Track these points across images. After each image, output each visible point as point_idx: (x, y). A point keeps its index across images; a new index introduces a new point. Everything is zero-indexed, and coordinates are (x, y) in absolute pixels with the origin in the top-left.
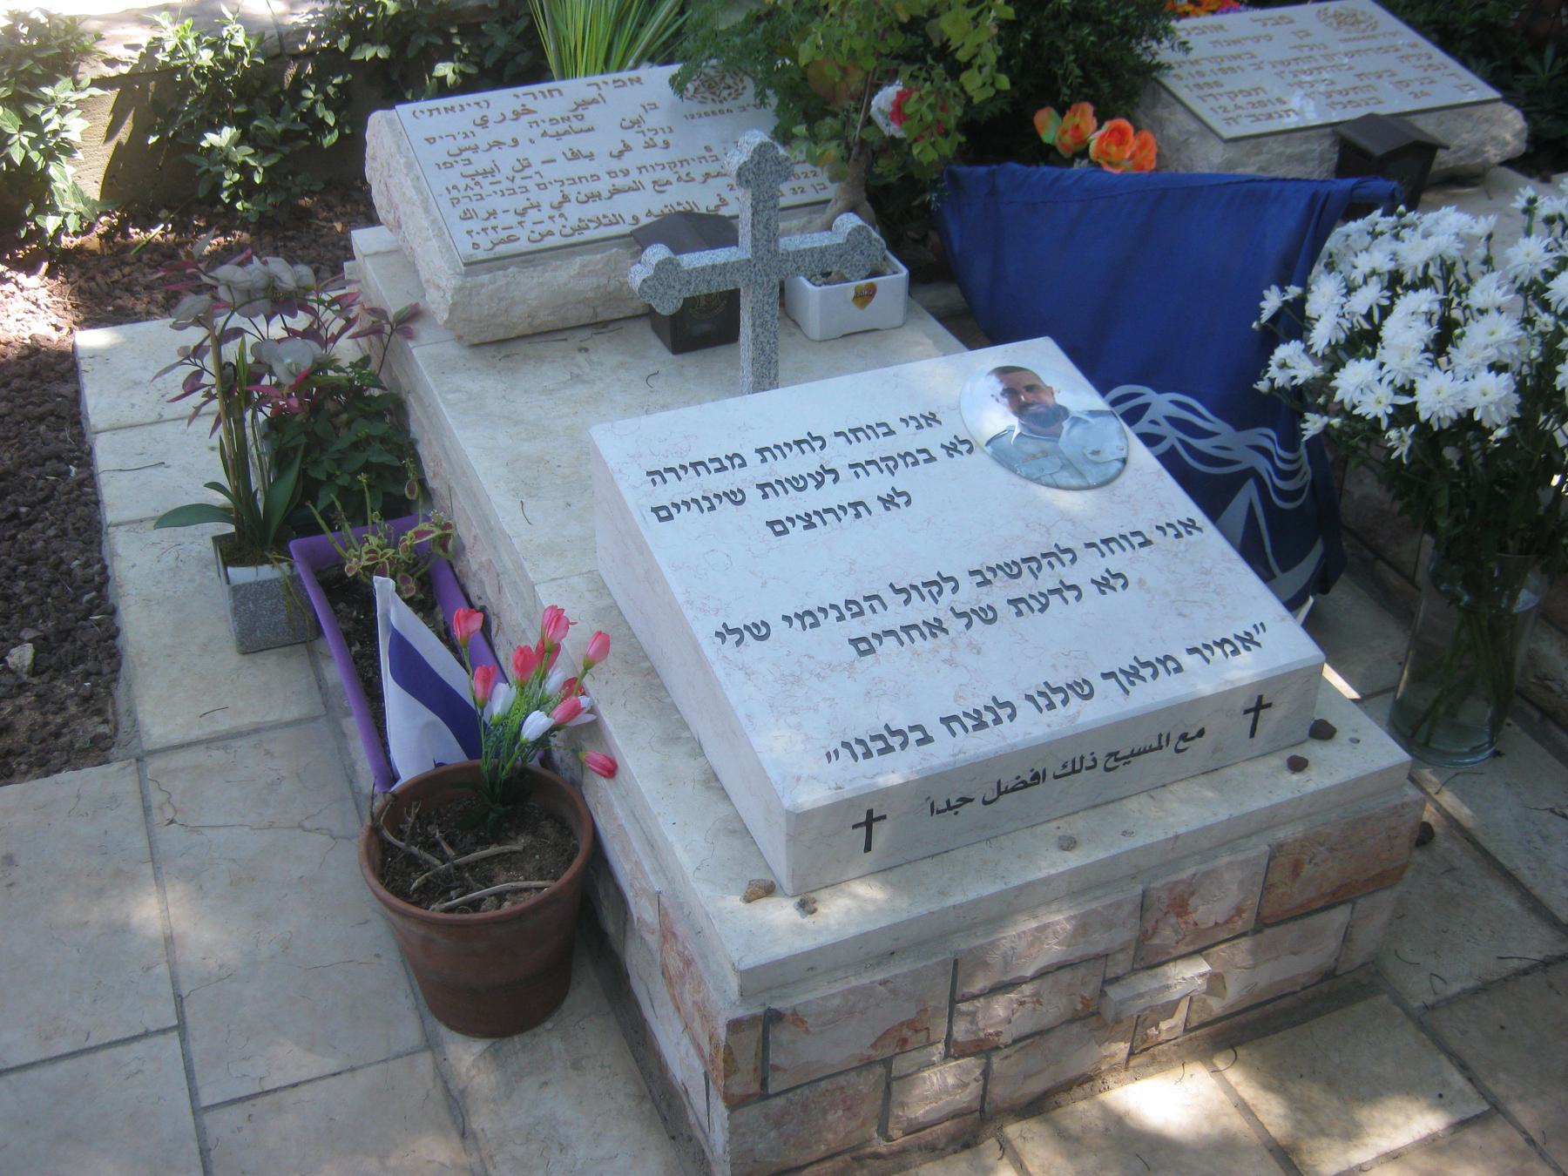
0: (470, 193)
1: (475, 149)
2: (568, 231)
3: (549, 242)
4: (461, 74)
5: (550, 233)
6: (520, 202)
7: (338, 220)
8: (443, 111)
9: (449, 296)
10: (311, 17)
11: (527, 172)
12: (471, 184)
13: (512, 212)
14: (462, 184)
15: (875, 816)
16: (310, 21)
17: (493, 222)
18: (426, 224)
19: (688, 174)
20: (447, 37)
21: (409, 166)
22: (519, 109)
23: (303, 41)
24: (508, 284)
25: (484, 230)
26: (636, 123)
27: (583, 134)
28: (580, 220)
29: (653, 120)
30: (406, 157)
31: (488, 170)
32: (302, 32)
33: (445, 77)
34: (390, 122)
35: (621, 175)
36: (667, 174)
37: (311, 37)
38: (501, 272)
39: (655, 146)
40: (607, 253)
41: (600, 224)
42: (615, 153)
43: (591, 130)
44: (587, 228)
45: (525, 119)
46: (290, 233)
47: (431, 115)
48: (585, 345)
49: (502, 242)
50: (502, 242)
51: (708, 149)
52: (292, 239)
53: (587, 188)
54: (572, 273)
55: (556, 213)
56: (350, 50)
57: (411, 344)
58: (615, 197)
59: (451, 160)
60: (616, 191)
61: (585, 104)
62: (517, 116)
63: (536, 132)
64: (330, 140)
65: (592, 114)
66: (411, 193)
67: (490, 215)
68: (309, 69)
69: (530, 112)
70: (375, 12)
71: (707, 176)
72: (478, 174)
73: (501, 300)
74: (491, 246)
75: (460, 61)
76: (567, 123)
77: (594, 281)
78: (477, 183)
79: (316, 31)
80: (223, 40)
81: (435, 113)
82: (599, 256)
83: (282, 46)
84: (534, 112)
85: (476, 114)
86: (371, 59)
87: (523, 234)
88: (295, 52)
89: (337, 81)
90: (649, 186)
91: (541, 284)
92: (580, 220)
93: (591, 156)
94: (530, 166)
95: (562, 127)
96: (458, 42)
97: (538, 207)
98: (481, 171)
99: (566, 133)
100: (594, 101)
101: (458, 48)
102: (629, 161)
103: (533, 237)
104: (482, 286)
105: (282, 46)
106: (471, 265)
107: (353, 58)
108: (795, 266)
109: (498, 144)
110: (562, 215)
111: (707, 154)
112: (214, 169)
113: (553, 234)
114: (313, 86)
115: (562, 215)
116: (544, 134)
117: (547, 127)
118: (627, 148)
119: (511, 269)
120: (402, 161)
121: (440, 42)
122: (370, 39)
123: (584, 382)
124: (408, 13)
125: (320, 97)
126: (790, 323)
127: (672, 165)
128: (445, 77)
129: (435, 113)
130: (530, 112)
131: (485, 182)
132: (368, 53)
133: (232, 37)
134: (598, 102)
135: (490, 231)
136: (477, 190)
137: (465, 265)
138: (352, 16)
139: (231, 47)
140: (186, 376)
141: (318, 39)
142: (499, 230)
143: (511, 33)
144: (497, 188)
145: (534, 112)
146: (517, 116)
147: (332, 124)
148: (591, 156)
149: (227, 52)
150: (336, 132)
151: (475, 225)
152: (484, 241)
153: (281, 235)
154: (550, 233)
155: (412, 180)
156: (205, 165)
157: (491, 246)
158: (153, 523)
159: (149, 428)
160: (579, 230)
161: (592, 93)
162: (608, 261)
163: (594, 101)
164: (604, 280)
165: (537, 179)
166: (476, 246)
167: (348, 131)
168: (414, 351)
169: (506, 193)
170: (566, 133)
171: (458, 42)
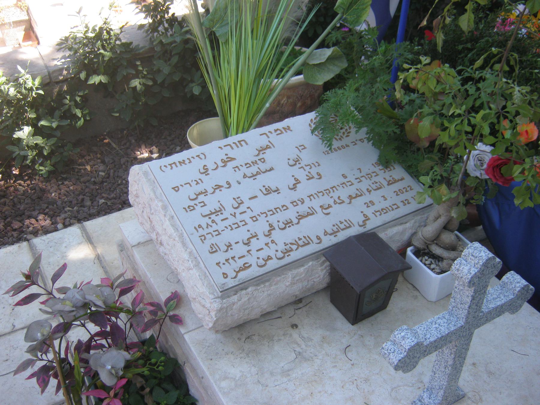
0: (210, 230)
1: (205, 193)
2: (280, 255)
3: (273, 264)
4: (144, 84)
5: (269, 258)
6: (242, 234)
7: (88, 164)
8: (178, 164)
9: (213, 314)
10: (63, 60)
11: (242, 208)
12: (210, 222)
13: (241, 243)
14: (204, 221)
15: (250, 252)
16: (64, 63)
17: (230, 254)
18: (186, 256)
19: (339, 198)
20: (135, 67)
21: (165, 208)
22: (225, 158)
23: (61, 75)
24: (249, 299)
25: (227, 260)
26: (297, 161)
27: (268, 173)
28: (286, 244)
29: (306, 157)
30: (161, 201)
31: (218, 209)
32: (61, 70)
33: (136, 87)
34: (146, 174)
35: (299, 203)
36: (326, 200)
37: (65, 72)
38: (244, 292)
39: (313, 178)
40: (306, 267)
41: (299, 246)
42: (291, 186)
43: (271, 169)
44: (292, 250)
45: (230, 165)
46: (65, 176)
47: (172, 168)
48: (295, 320)
49: (242, 269)
50: (242, 269)
51: (344, 176)
52: (66, 179)
53: (283, 216)
54: (287, 284)
55: (268, 240)
56: (87, 79)
57: (182, 330)
58: (301, 221)
59: (192, 203)
60: (300, 217)
61: (262, 150)
62: (225, 163)
63: (239, 175)
64: (81, 122)
65: (268, 155)
66: (171, 230)
67: (228, 246)
68: (65, 88)
69: (232, 159)
70: (99, 59)
71: (351, 197)
72: (212, 213)
73: (245, 310)
74: (235, 274)
75: (143, 78)
76: (256, 166)
77: (300, 285)
78: (213, 221)
79: (67, 69)
80: (21, 85)
81: (174, 166)
82: (302, 269)
83: (50, 78)
84: (234, 159)
85: (198, 164)
86: (98, 84)
87: (251, 260)
88: (57, 80)
89: (81, 94)
90: (319, 210)
91: (270, 295)
92: (286, 244)
93: (277, 191)
94: (242, 203)
95: (254, 169)
96: (141, 68)
97: (255, 236)
98: (213, 211)
99: (258, 173)
100: (268, 147)
101: (141, 72)
102: (304, 190)
103: (261, 262)
104: (234, 304)
105: (50, 78)
106: (226, 293)
107: (88, 83)
108: (486, 319)
109: (218, 187)
110: (273, 242)
111: (345, 181)
112: (22, 153)
113: (271, 258)
114: (68, 97)
115: (273, 242)
116: (245, 176)
117: (244, 169)
118: (298, 181)
119: (250, 289)
120: (160, 204)
121: (134, 72)
122: (96, 72)
123: (306, 360)
124: (115, 58)
125: (73, 103)
126: (410, 286)
127: (327, 191)
128: (136, 87)
129: (174, 166)
130: (232, 159)
131: (218, 219)
132: (96, 79)
133: (25, 83)
134: (270, 148)
135: (231, 261)
136: (215, 227)
137: (221, 292)
138: (86, 62)
139: (25, 88)
140: (28, 346)
141: (69, 73)
142: (236, 259)
143: (170, 65)
144: (226, 223)
145: (234, 159)
146: (225, 163)
147: (80, 116)
148: (277, 191)
149: (24, 91)
150: (82, 119)
151: (220, 257)
152: (229, 269)
153: (60, 178)
154: (269, 258)
155: (169, 220)
156: (17, 151)
157: (235, 274)
158: (13, 374)
159: (8, 337)
160: (287, 252)
161: (264, 141)
162: (308, 271)
163: (268, 147)
164: (305, 283)
165: (249, 214)
166: (225, 275)
167: (88, 118)
168: (186, 337)
169: (233, 227)
170: (258, 173)
171: (141, 68)
